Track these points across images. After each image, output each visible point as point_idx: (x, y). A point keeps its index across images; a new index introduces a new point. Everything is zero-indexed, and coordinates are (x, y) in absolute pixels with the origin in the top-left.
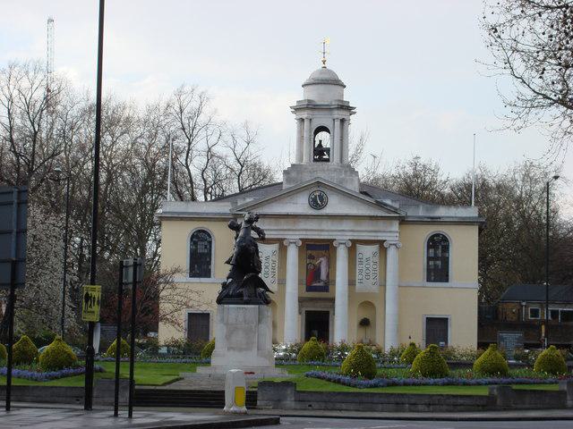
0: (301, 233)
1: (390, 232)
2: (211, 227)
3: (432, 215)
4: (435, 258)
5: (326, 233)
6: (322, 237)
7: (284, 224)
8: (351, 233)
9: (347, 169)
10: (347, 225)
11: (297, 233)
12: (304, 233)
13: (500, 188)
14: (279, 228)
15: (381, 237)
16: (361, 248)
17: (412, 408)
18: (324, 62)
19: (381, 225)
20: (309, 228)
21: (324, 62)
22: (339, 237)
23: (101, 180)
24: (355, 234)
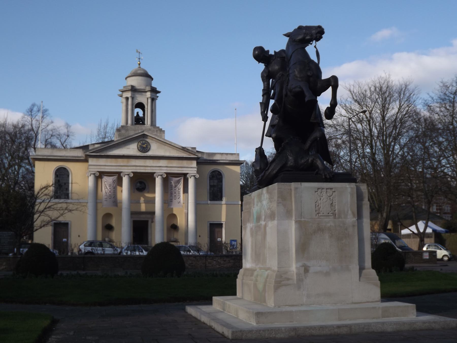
0: (132, 168)
1: (191, 168)
2: (69, 166)
3: (211, 159)
4: (375, 239)
5: (149, 168)
6: (147, 171)
7: (120, 162)
8: (165, 168)
9: (157, 129)
10: (163, 163)
11: (130, 168)
12: (134, 168)
13: (15, 127)
14: (118, 164)
15: (185, 171)
16: (174, 180)
17: (110, 185)
18: (139, 64)
19: (185, 163)
20: (137, 164)
21: (139, 64)
22: (157, 171)
23: (399, 129)
24: (168, 169)
